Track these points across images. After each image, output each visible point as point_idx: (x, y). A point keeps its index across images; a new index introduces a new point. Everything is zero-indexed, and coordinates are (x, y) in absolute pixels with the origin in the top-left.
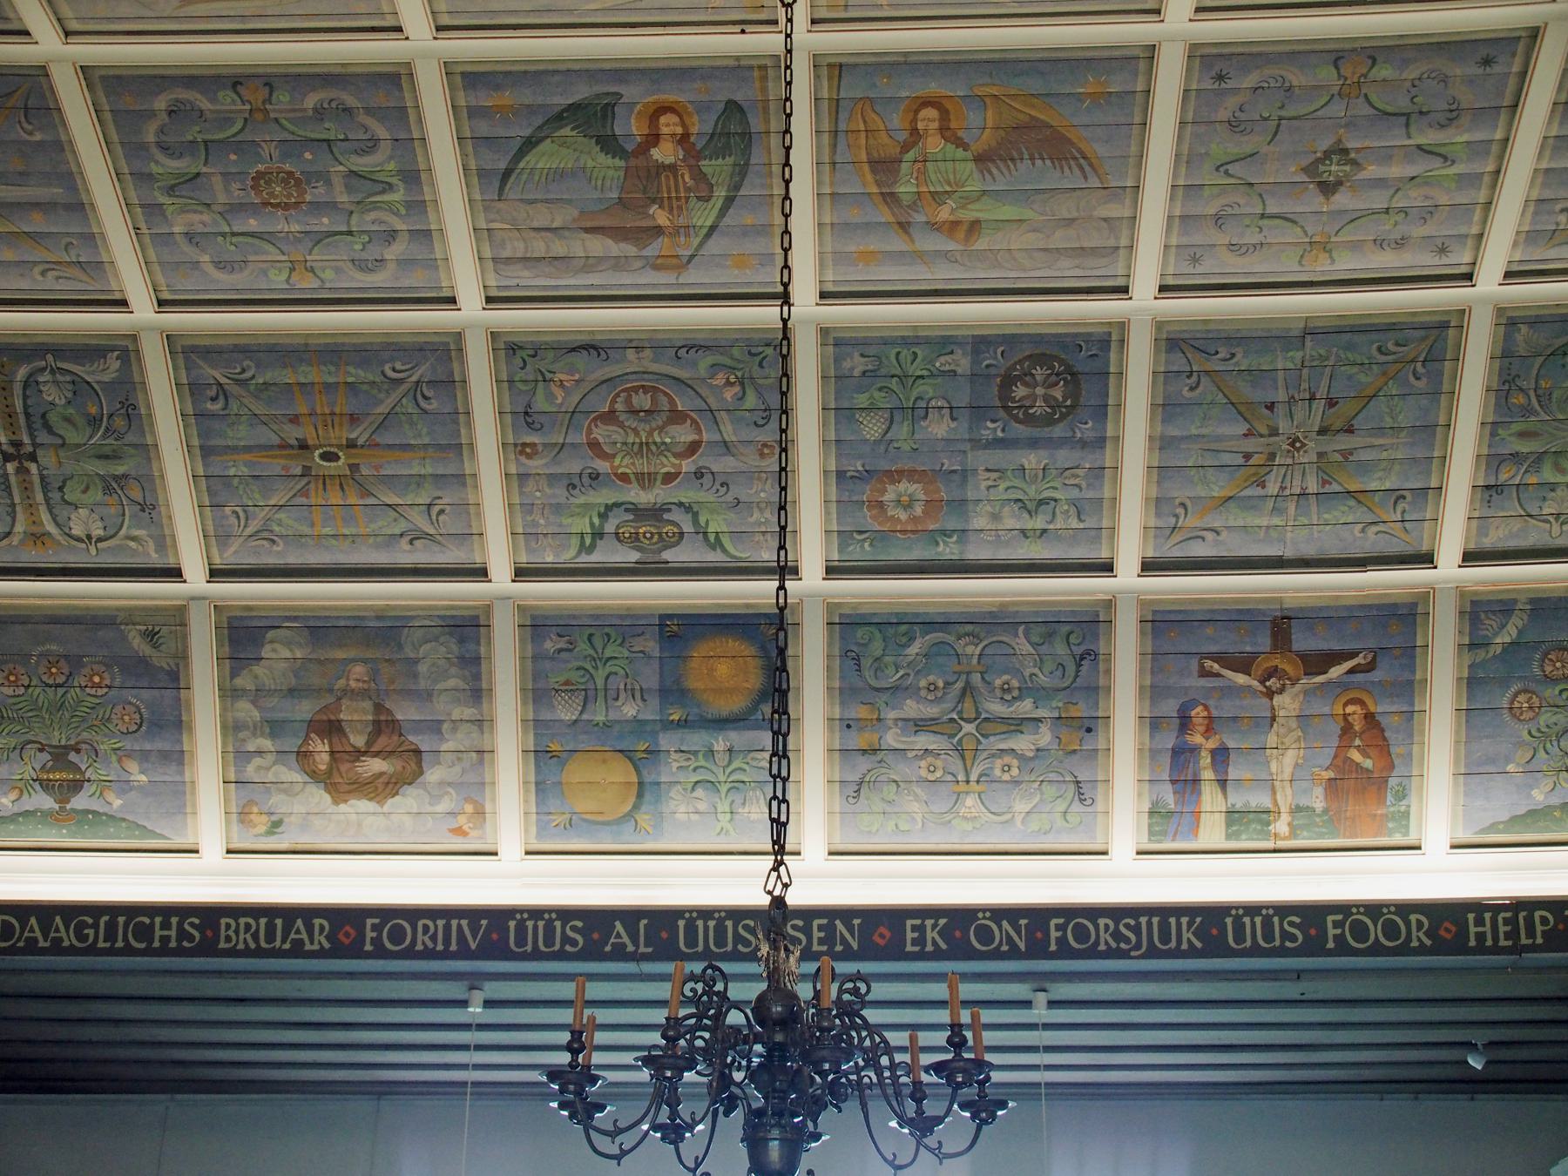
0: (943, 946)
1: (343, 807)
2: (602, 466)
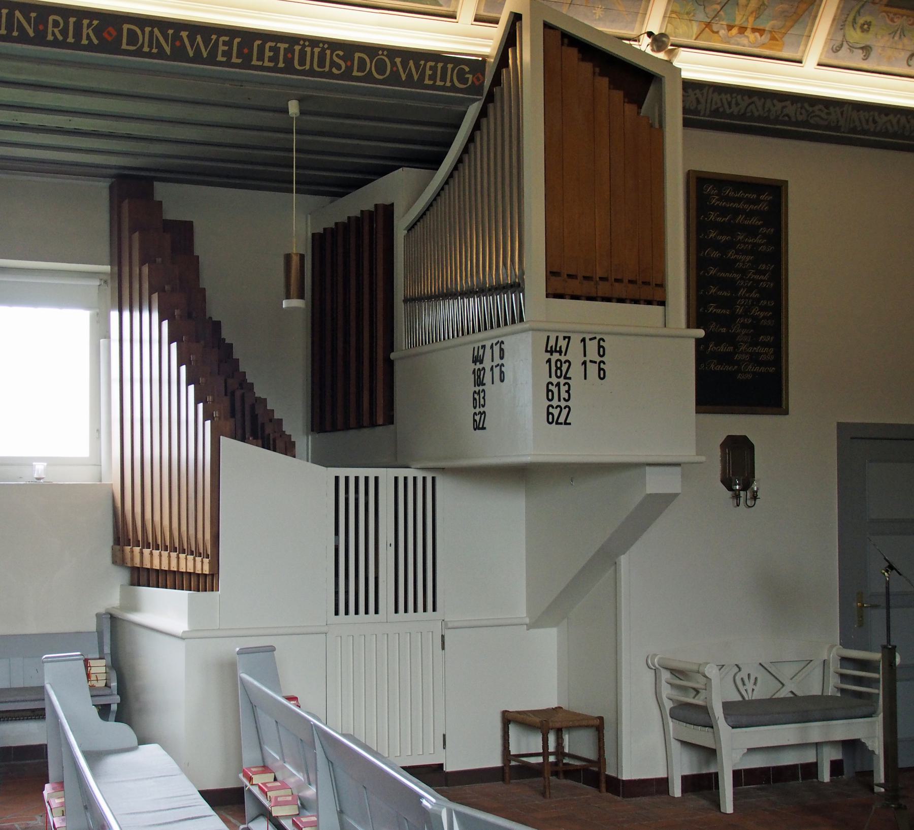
0: (96, 42)
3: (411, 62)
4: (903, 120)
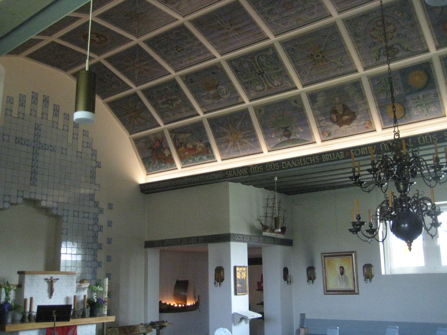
1: (342, 128)
2: (376, 40)
4: (167, 183)
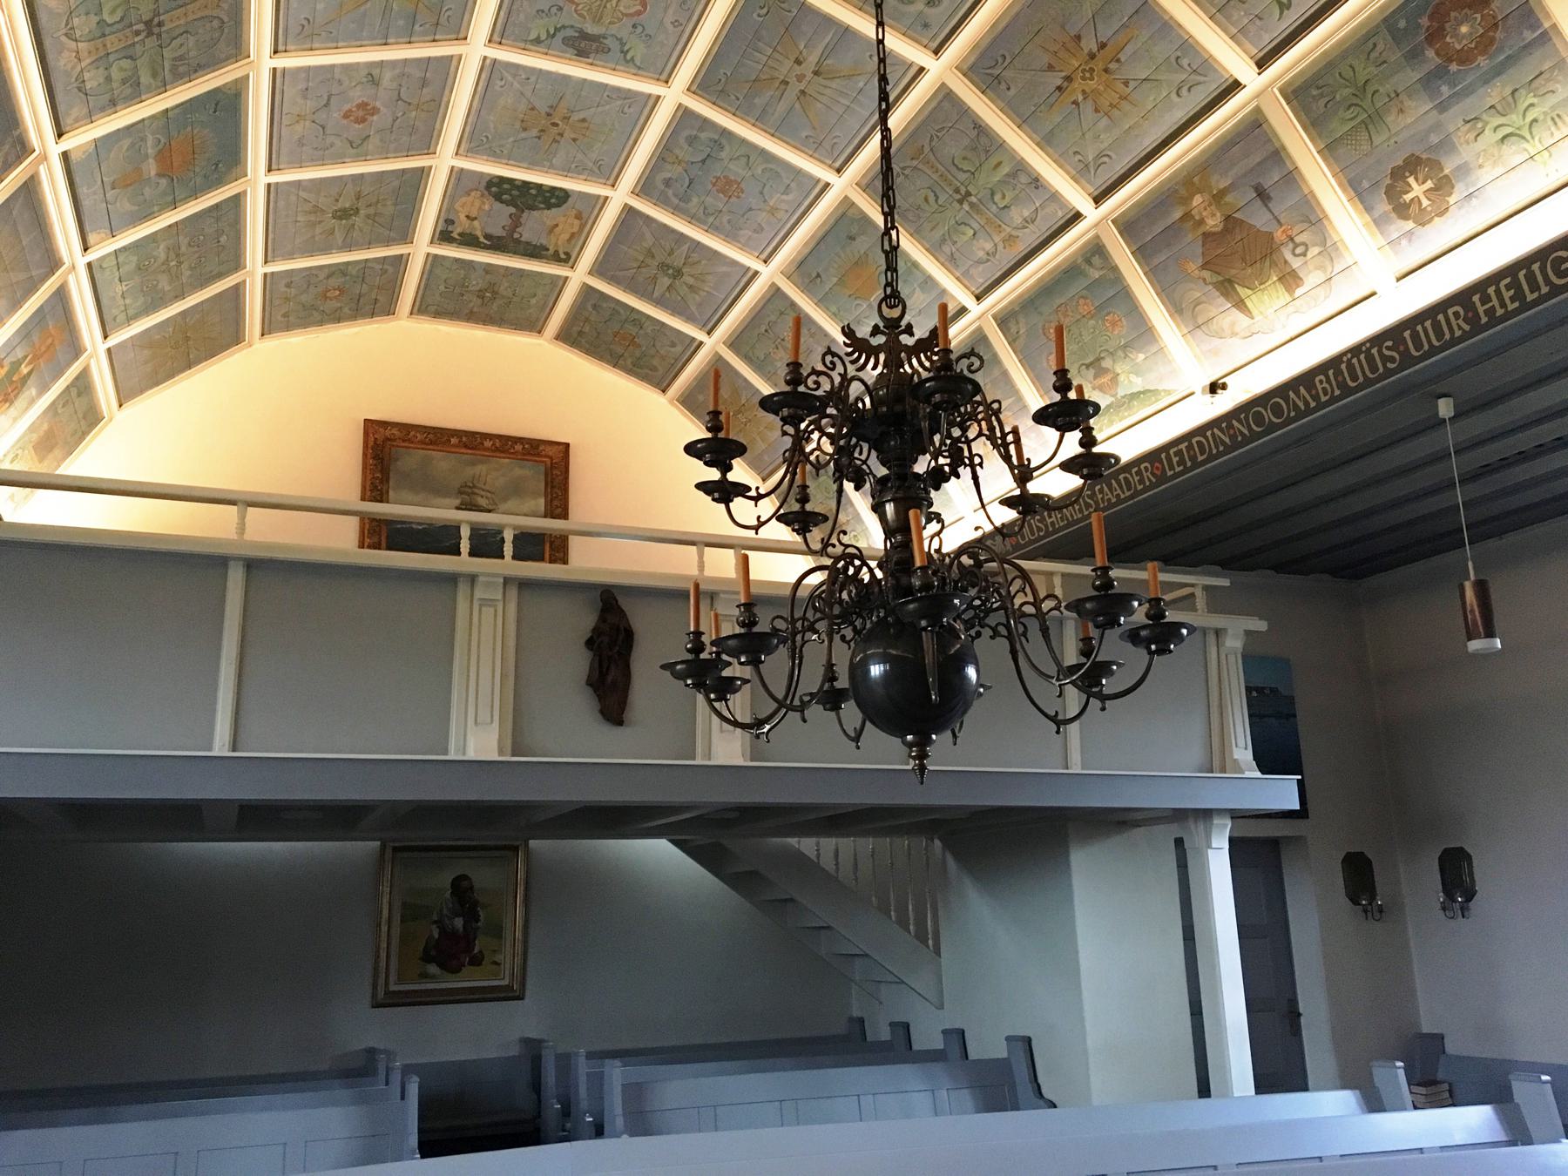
3: (1292, 394)
4: (395, 431)
